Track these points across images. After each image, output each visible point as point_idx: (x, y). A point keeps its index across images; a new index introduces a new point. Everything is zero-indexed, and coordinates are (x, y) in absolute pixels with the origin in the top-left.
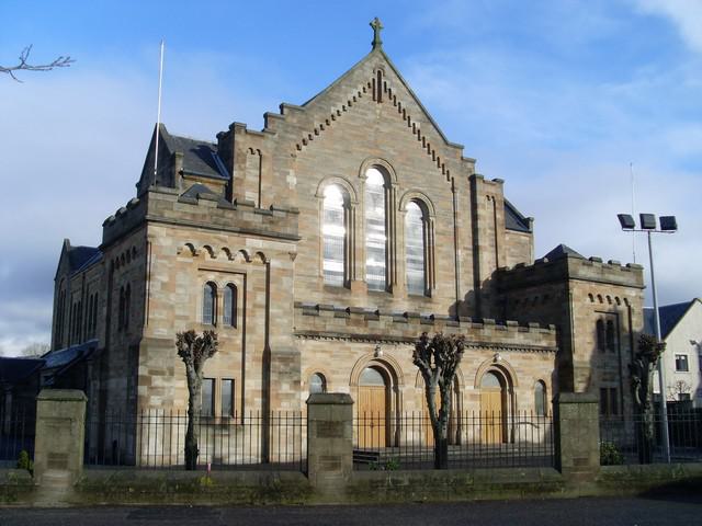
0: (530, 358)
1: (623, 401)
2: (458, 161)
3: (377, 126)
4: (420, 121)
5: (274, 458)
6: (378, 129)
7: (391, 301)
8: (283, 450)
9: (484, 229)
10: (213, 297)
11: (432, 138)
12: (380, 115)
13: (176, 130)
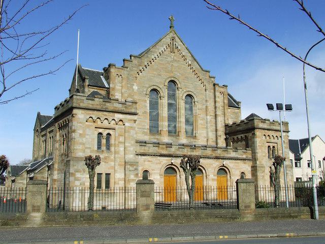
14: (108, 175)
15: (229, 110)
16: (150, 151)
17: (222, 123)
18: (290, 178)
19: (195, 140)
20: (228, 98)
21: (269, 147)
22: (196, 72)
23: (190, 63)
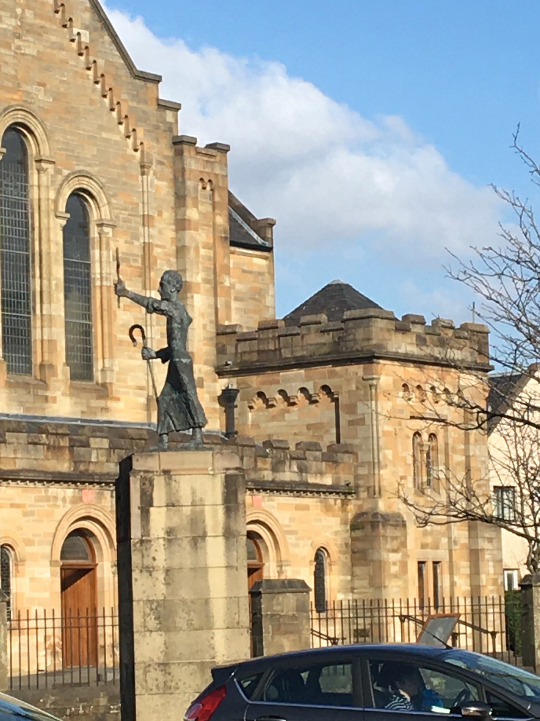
0: (306, 508)
1: (453, 584)
2: (152, 108)
3: (17, 42)
4: (86, 28)
5: (65, 682)
6: (19, 48)
7: (46, 399)
8: (42, 660)
9: (197, 249)
10: (469, 466)
11: (107, 61)
12: (22, 18)
13: (489, 335)
14: (435, 563)
15: (233, 260)
16: (20, 465)
17: (206, 321)
18: (491, 570)
19: (101, 403)
20: (229, 209)
21: (417, 434)
22: (109, 82)
23: (85, 38)
